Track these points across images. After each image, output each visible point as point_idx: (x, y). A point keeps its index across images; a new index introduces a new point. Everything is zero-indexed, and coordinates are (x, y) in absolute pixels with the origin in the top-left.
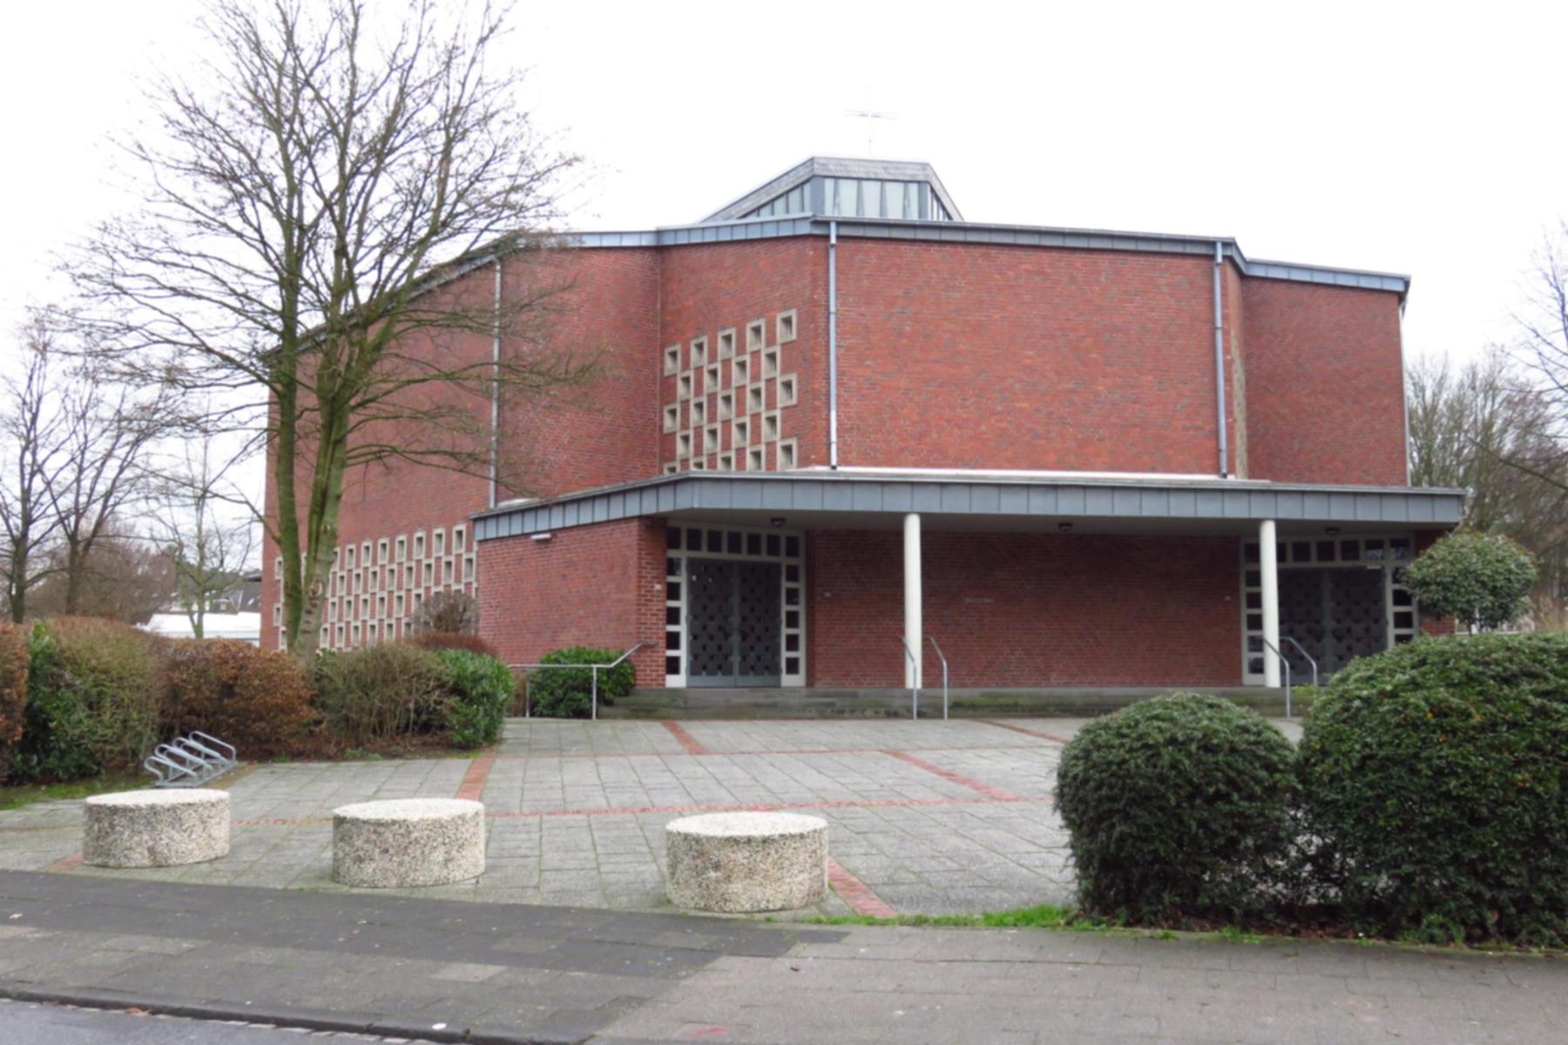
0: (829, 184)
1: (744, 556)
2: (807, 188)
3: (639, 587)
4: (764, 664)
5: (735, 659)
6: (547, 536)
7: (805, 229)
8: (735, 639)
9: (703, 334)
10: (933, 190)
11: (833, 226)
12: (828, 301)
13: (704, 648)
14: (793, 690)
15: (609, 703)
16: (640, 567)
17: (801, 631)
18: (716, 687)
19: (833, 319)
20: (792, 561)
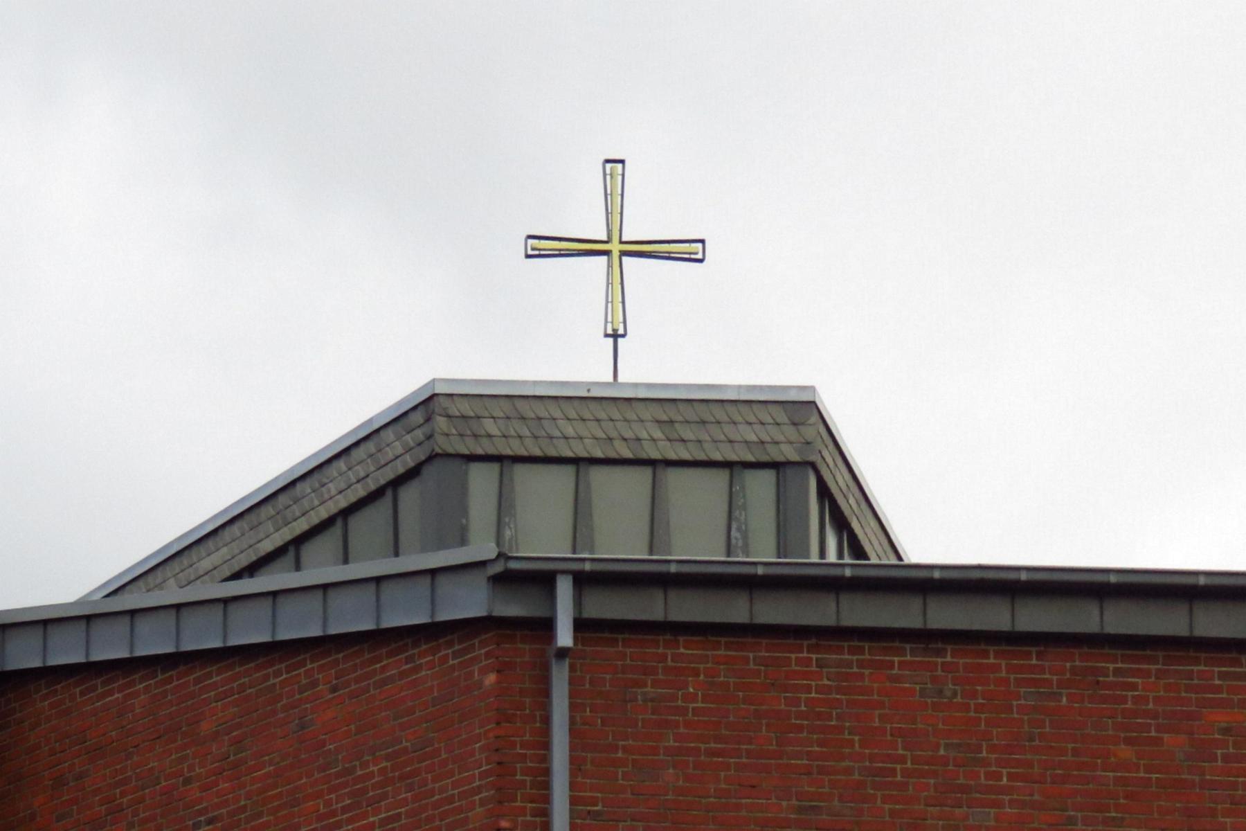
0: (482, 480)
2: (409, 495)
7: (469, 601)
10: (824, 492)
11: (564, 589)
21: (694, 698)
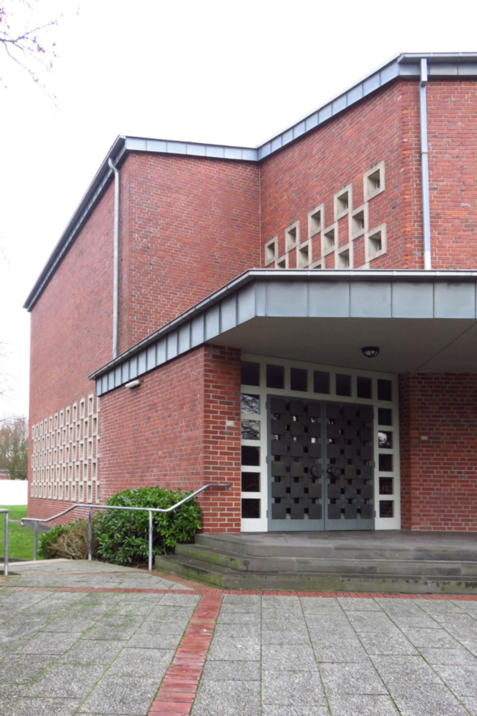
1: (332, 397)
3: (207, 422)
4: (354, 505)
5: (324, 502)
6: (136, 382)
8: (324, 481)
9: (295, 220)
12: (419, 145)
13: (288, 490)
14: (388, 533)
15: (170, 550)
16: (207, 401)
17: (395, 474)
18: (311, 544)
19: (425, 159)
20: (385, 405)
21: (467, 101)
